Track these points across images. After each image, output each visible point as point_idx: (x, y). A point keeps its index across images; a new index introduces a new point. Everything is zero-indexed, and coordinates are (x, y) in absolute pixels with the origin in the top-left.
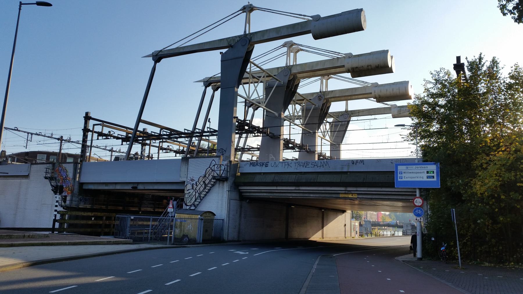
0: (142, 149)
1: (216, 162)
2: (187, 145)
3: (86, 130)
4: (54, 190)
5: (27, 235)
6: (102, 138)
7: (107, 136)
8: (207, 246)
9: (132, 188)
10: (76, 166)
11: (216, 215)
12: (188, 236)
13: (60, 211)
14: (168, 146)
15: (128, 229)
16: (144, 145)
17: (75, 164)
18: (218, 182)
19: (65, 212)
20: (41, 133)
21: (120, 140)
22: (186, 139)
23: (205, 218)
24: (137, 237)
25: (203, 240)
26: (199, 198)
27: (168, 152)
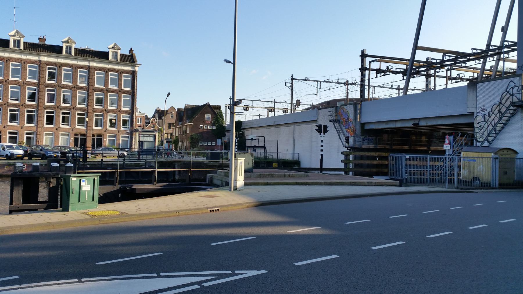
0: (427, 81)
1: (515, 84)
2: (480, 70)
3: (363, 69)
4: (318, 130)
5: (287, 174)
6: (381, 75)
7: (385, 72)
8: (505, 192)
9: (412, 124)
10: (356, 107)
11: (518, 153)
12: (478, 178)
13: (344, 152)
14: (458, 75)
15: (404, 170)
16: (428, 76)
17: (355, 105)
18: (520, 109)
19: (348, 153)
20: (328, 80)
21: (401, 75)
22: (478, 61)
23: (501, 157)
24: (420, 178)
25: (500, 185)
26: (494, 132)
27: (458, 82)
